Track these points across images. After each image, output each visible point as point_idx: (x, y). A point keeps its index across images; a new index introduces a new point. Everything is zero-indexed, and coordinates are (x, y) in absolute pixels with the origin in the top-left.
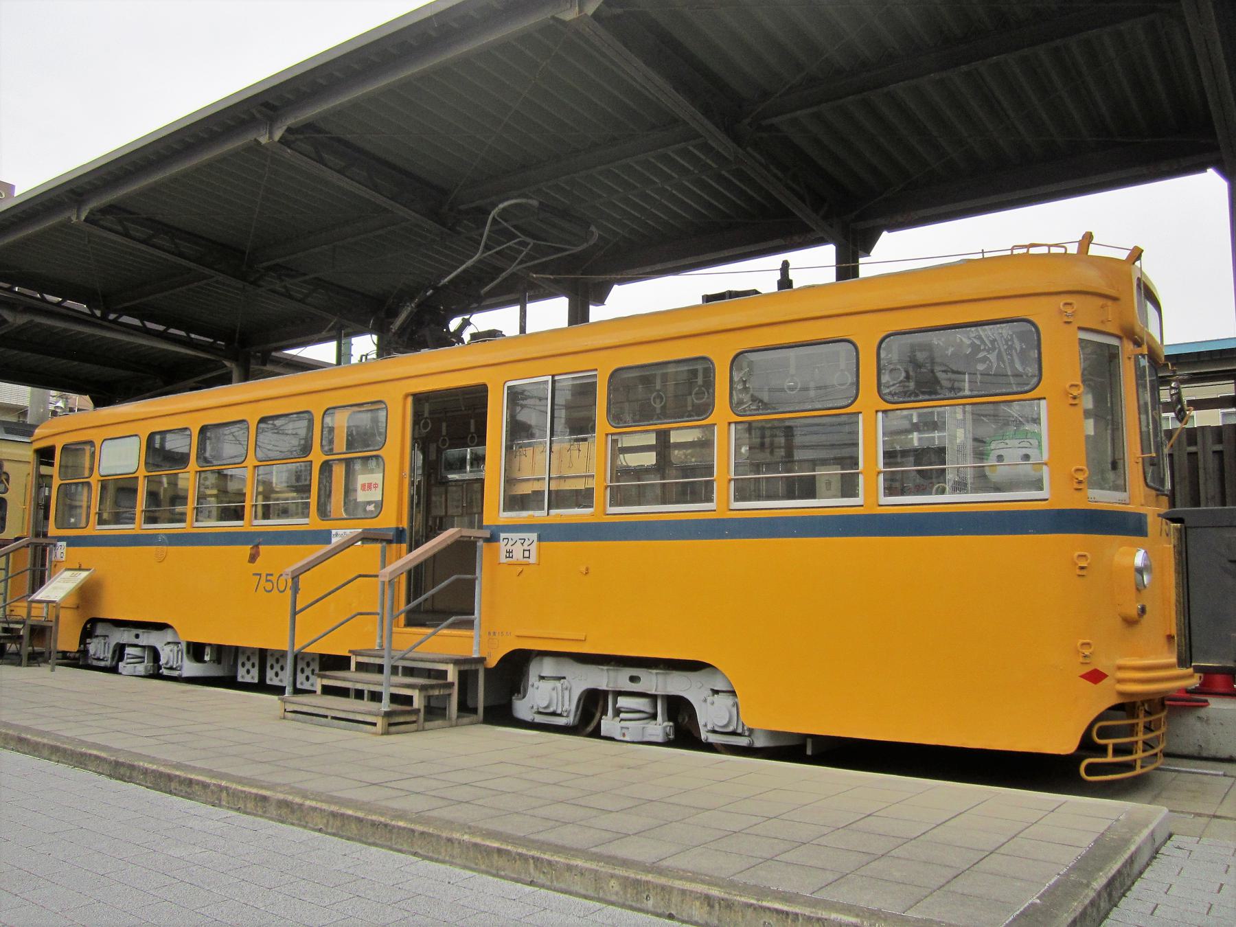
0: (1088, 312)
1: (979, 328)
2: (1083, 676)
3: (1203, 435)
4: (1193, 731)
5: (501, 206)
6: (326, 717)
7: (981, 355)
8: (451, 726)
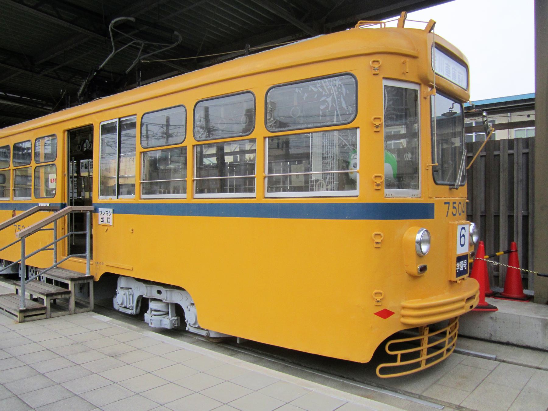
0: (391, 66)
1: (322, 81)
2: (376, 314)
3: (518, 143)
4: (485, 326)
5: (113, 22)
6: (3, 309)
7: (323, 99)
8: (71, 314)
